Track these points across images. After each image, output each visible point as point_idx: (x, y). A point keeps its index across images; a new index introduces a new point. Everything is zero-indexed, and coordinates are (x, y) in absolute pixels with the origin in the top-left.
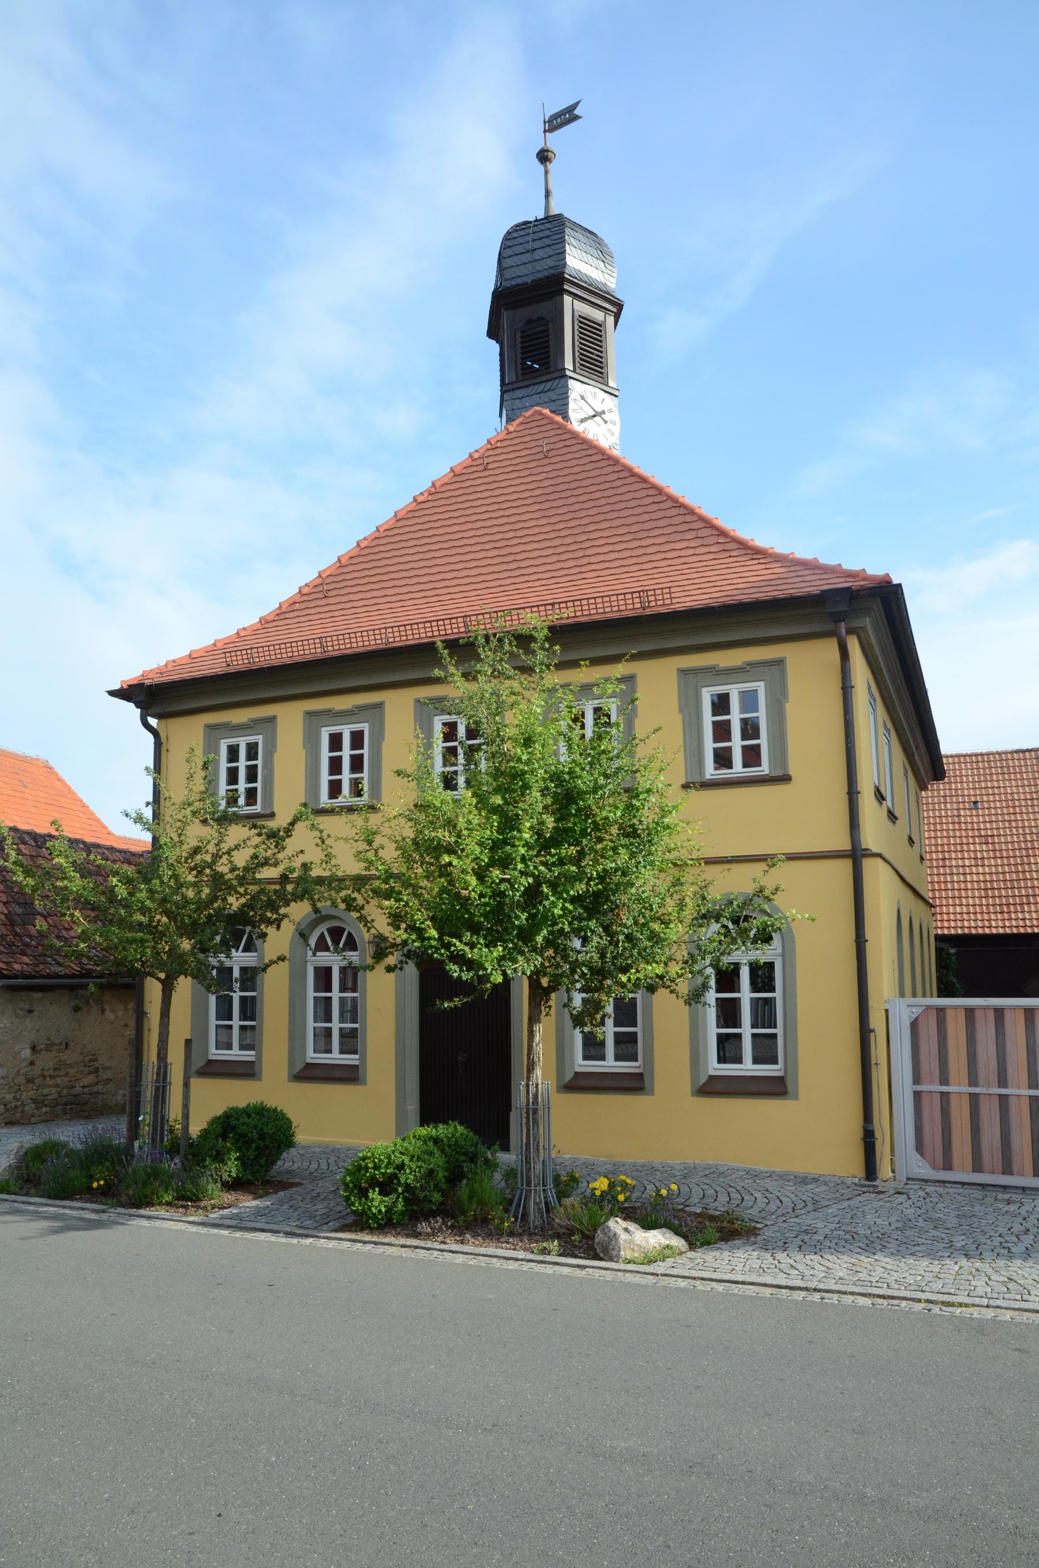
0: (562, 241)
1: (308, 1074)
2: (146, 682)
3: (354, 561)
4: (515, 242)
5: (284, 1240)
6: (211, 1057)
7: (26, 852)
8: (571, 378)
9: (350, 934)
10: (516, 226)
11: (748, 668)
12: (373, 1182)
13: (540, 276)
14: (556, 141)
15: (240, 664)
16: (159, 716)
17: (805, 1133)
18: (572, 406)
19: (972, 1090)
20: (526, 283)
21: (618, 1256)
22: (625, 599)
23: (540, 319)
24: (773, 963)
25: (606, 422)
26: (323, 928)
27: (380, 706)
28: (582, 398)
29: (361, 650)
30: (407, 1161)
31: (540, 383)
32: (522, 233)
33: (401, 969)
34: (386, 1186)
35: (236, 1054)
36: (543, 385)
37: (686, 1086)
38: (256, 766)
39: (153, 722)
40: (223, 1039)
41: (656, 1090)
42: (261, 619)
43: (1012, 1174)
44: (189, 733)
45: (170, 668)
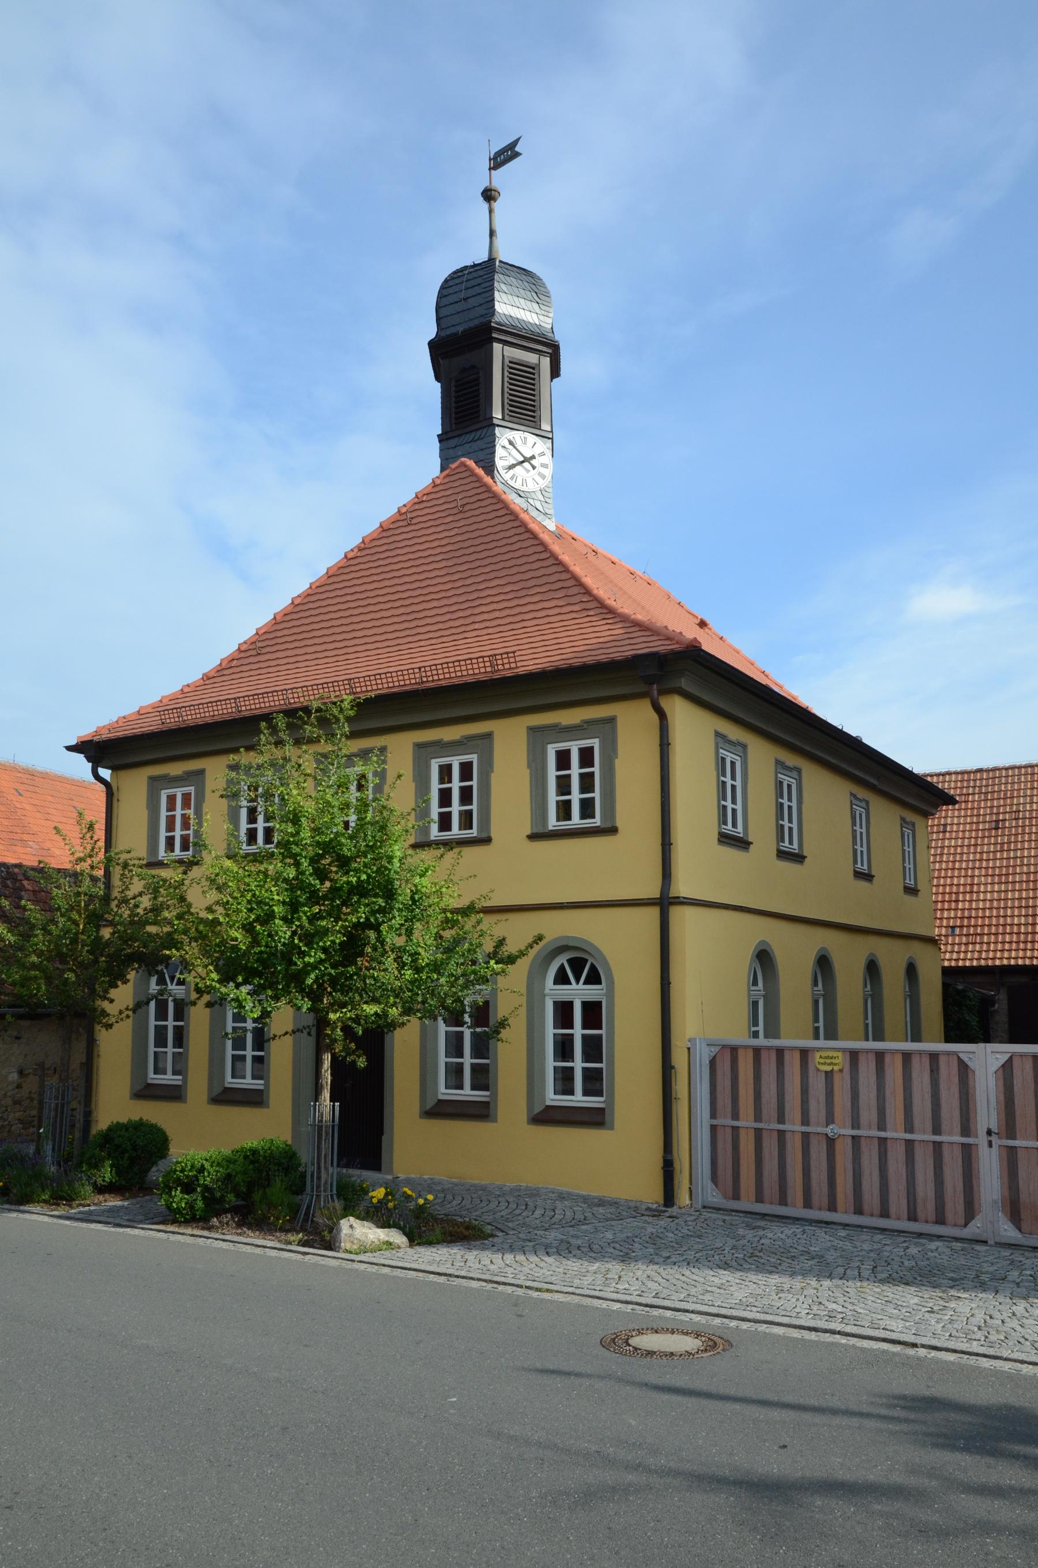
0: (491, 289)
2: (95, 739)
3: (288, 618)
4: (450, 291)
5: (113, 1229)
7: (30, 888)
8: (498, 426)
9: (593, 966)
10: (455, 273)
11: (585, 726)
12: (179, 1182)
13: (472, 324)
14: (501, 178)
15: (172, 721)
16: (114, 768)
17: (617, 1160)
18: (499, 452)
20: (455, 334)
21: (339, 1247)
23: (473, 367)
25: (534, 468)
26: (562, 960)
27: (489, 736)
28: (511, 443)
30: (207, 1165)
31: (471, 432)
32: (457, 281)
33: (221, 1005)
34: (188, 1188)
35: (248, 1082)
36: (473, 434)
37: (522, 1115)
38: (592, 774)
39: (105, 773)
40: (239, 1064)
42: (204, 675)
43: (786, 1205)
44: (134, 786)
45: (121, 724)
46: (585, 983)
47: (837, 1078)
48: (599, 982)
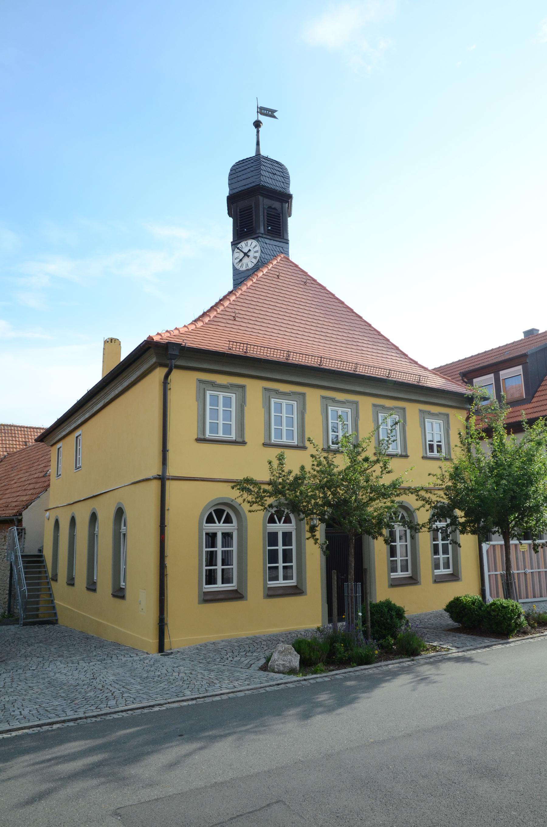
1: (395, 584)
6: (205, 590)
19: (532, 571)
22: (254, 348)
24: (277, 533)
29: (296, 362)
41: (422, 583)
46: (224, 523)
47: (526, 552)
48: (291, 522)
